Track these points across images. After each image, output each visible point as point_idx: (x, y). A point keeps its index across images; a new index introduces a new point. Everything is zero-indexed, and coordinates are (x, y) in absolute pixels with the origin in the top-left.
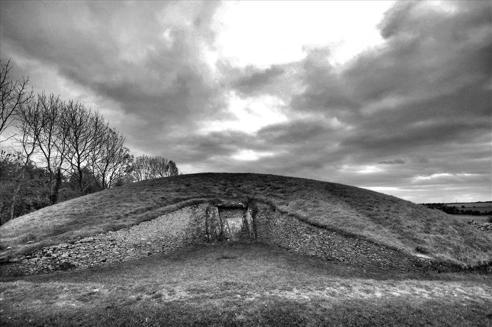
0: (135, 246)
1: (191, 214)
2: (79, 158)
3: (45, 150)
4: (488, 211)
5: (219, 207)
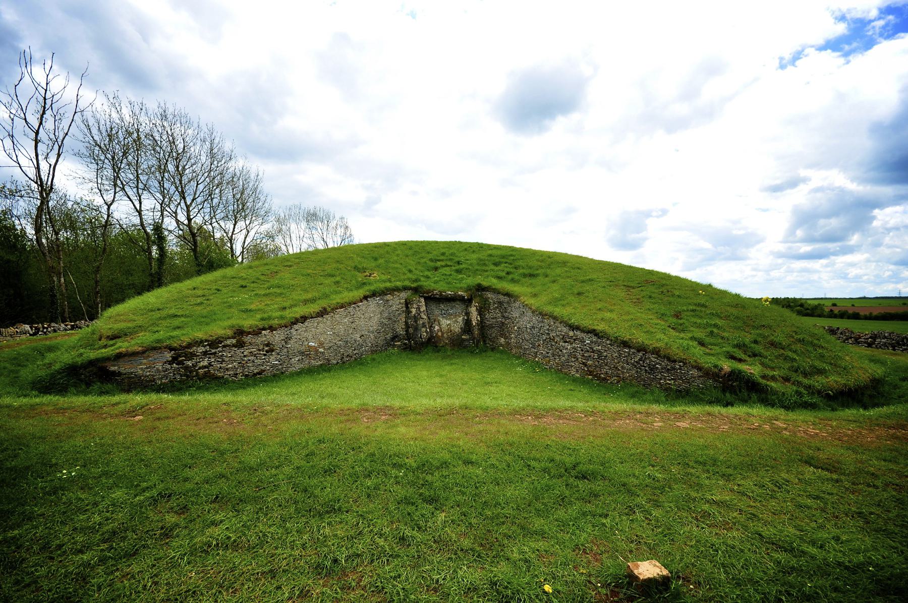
0: (302, 353)
1: (382, 308)
2: (188, 211)
3: (134, 198)
4: (901, 310)
5: (426, 299)
